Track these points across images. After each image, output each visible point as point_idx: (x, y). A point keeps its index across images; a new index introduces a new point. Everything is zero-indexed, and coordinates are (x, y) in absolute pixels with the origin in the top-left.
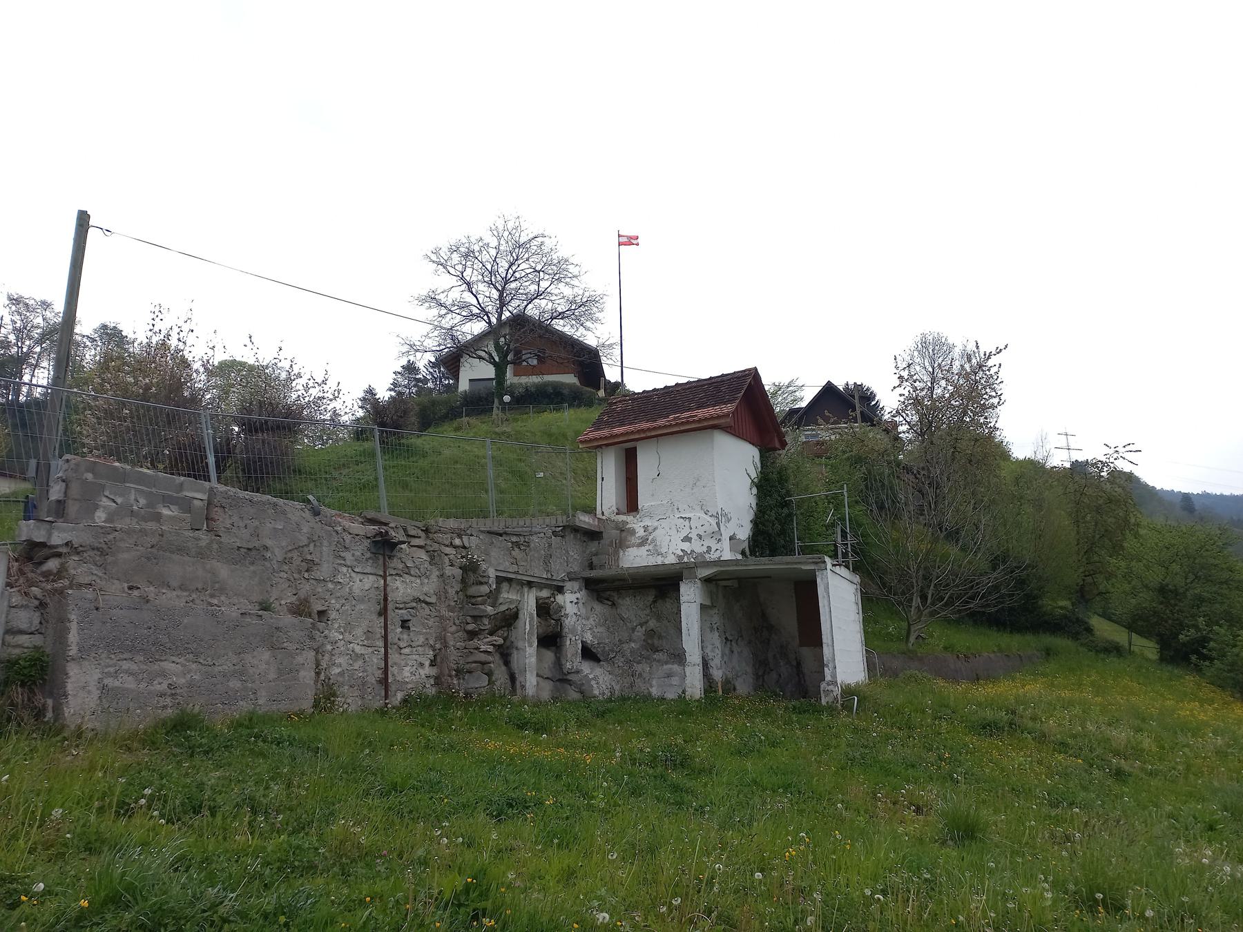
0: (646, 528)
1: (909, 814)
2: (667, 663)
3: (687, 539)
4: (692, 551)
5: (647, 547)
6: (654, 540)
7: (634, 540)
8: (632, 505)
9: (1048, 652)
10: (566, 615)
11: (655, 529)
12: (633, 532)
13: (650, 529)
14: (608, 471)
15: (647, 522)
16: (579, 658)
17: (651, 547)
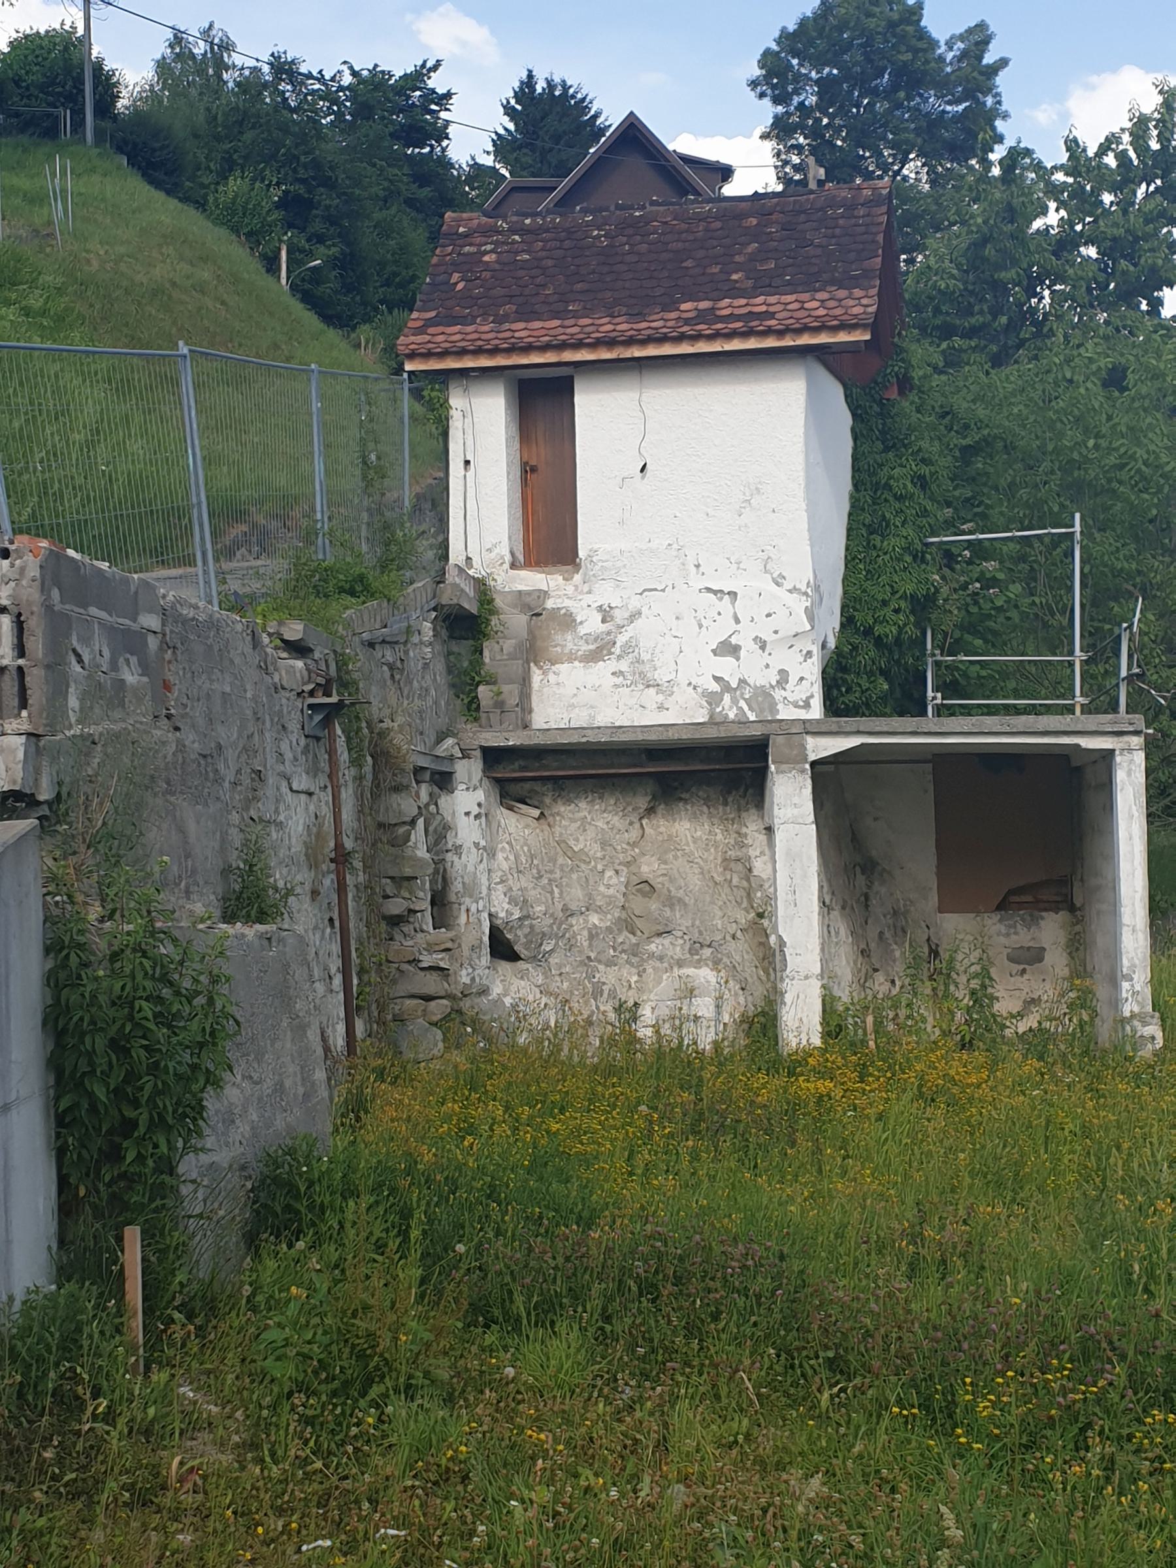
0: (606, 614)
1: (383, 1282)
2: (680, 964)
3: (729, 649)
4: (742, 681)
5: (611, 665)
6: (628, 648)
7: (568, 642)
8: (550, 531)
9: (1082, 880)
10: (458, 849)
11: (635, 616)
12: (568, 621)
13: (619, 616)
14: (482, 424)
15: (605, 594)
16: (485, 959)
17: (624, 666)
